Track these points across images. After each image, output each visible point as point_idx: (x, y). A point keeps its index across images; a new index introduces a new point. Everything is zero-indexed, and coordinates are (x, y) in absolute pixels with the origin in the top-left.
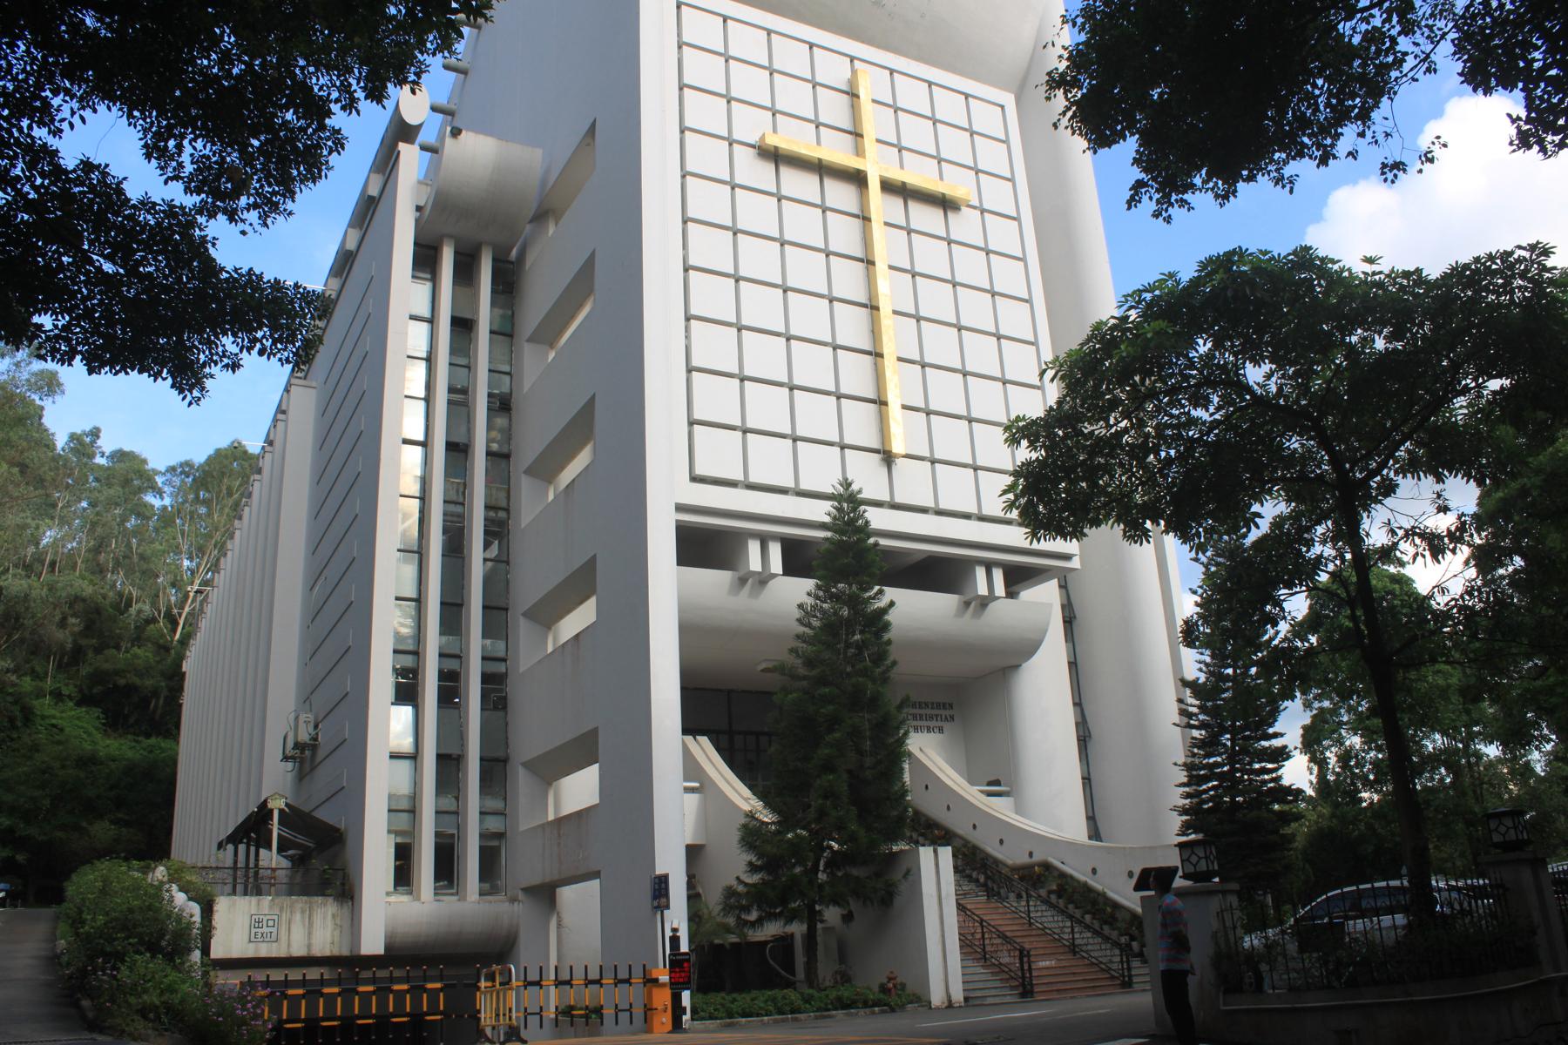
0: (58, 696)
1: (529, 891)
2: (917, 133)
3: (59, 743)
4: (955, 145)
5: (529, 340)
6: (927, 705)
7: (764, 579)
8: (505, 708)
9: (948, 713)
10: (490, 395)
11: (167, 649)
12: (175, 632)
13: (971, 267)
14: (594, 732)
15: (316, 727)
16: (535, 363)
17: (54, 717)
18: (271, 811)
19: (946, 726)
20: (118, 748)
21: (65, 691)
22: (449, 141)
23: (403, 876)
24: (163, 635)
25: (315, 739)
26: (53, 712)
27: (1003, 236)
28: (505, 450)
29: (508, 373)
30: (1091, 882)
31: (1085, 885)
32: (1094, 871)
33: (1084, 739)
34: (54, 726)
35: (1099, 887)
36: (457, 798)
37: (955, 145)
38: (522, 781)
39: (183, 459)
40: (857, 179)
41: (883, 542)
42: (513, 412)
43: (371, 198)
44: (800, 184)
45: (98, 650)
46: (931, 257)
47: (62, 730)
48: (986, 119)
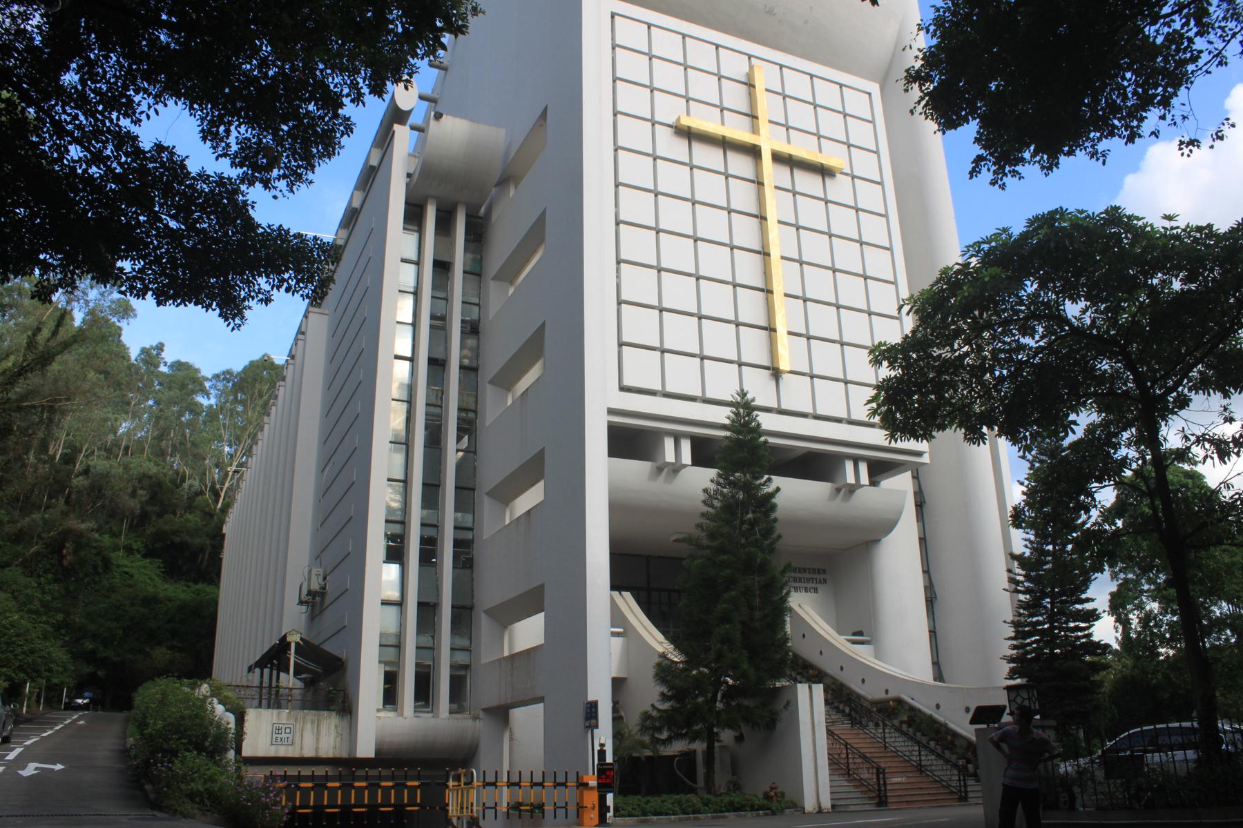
0: (129, 550)
1: (485, 710)
2: (801, 116)
3: (130, 586)
4: (831, 124)
5: (496, 278)
6: (805, 570)
7: (676, 468)
8: (471, 567)
9: (821, 577)
12: (217, 502)
13: (843, 222)
14: (542, 587)
15: (325, 578)
17: (126, 566)
18: (289, 643)
19: (820, 587)
20: (177, 592)
21: (135, 547)
22: (432, 122)
23: (390, 697)
24: (208, 505)
25: (324, 588)
26: (125, 562)
27: (870, 197)
28: (474, 365)
30: (936, 716)
32: (938, 706)
33: (931, 600)
35: (942, 719)
36: (433, 637)
37: (831, 124)
38: (484, 625)
39: (224, 369)
40: (754, 152)
41: (771, 440)
42: (481, 335)
43: (372, 168)
44: (707, 156)
45: (160, 515)
46: (811, 213)
47: (132, 576)
48: (857, 103)
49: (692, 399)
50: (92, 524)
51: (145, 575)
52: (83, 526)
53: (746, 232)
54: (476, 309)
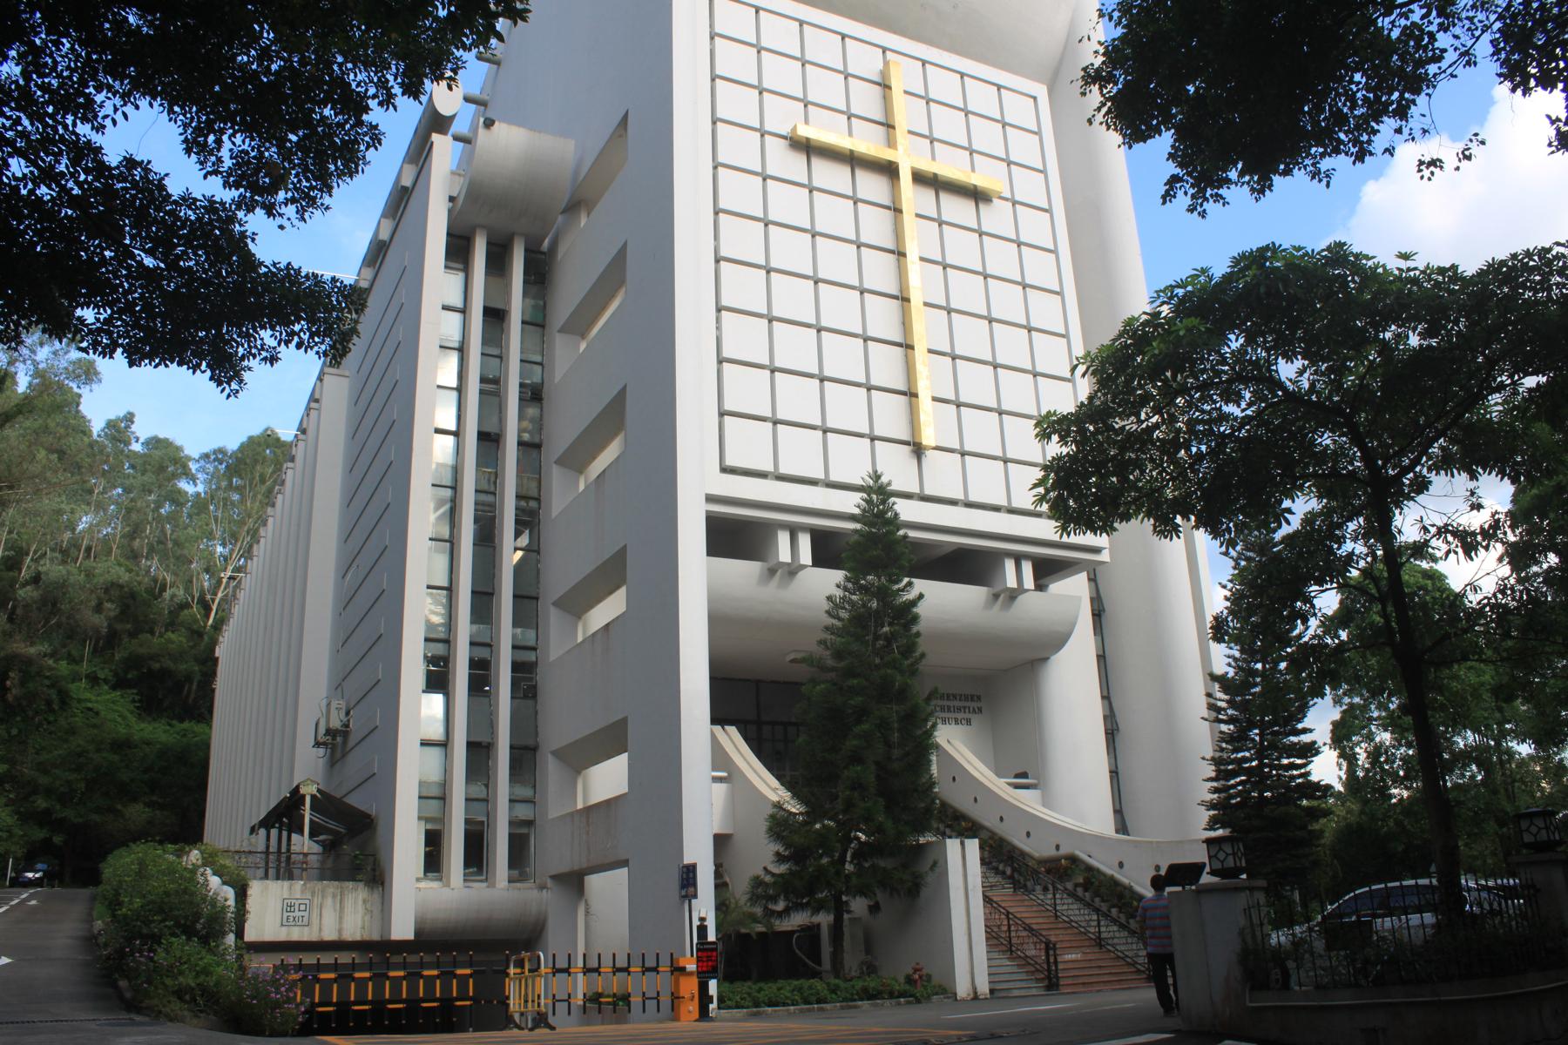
0: (94, 680)
2: (949, 125)
3: (94, 726)
4: (987, 136)
6: (955, 697)
7: (793, 570)
8: (534, 696)
10: (522, 385)
11: (200, 634)
12: (208, 617)
13: (1002, 259)
14: (624, 721)
15: (348, 713)
16: (566, 354)
18: (303, 797)
19: (975, 718)
20: (159, 732)
21: (101, 675)
22: (481, 131)
23: (433, 862)
25: (347, 726)
26: (88, 695)
27: (1035, 227)
28: (537, 440)
29: (540, 364)
30: (1117, 876)
31: (1112, 877)
32: (1121, 865)
33: (1112, 733)
34: (90, 709)
35: (1125, 881)
36: (487, 786)
37: (987, 136)
38: (551, 769)
39: (216, 446)
40: (889, 170)
41: (912, 534)
43: (405, 189)
44: (831, 175)
45: (133, 635)
46: (962, 248)
47: (97, 713)
48: (1019, 110)
49: (813, 482)
50: (44, 648)
51: (116, 712)
52: (32, 650)
53: (879, 271)
54: (538, 369)
